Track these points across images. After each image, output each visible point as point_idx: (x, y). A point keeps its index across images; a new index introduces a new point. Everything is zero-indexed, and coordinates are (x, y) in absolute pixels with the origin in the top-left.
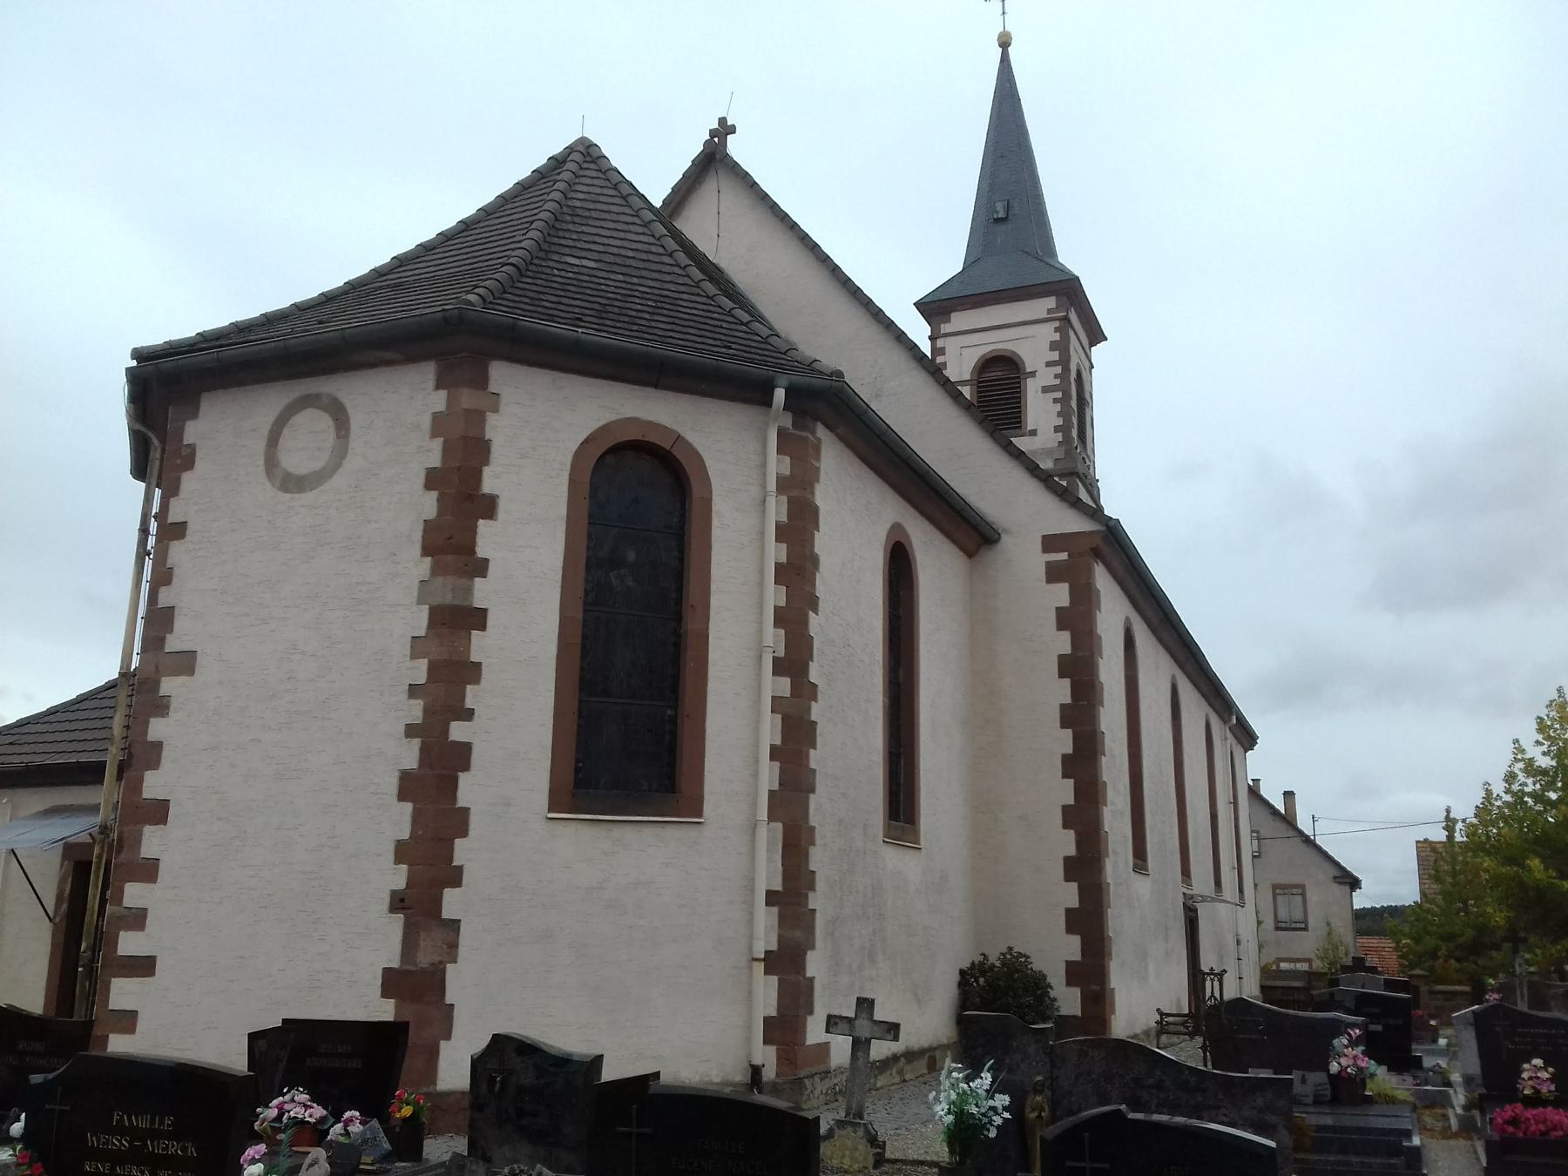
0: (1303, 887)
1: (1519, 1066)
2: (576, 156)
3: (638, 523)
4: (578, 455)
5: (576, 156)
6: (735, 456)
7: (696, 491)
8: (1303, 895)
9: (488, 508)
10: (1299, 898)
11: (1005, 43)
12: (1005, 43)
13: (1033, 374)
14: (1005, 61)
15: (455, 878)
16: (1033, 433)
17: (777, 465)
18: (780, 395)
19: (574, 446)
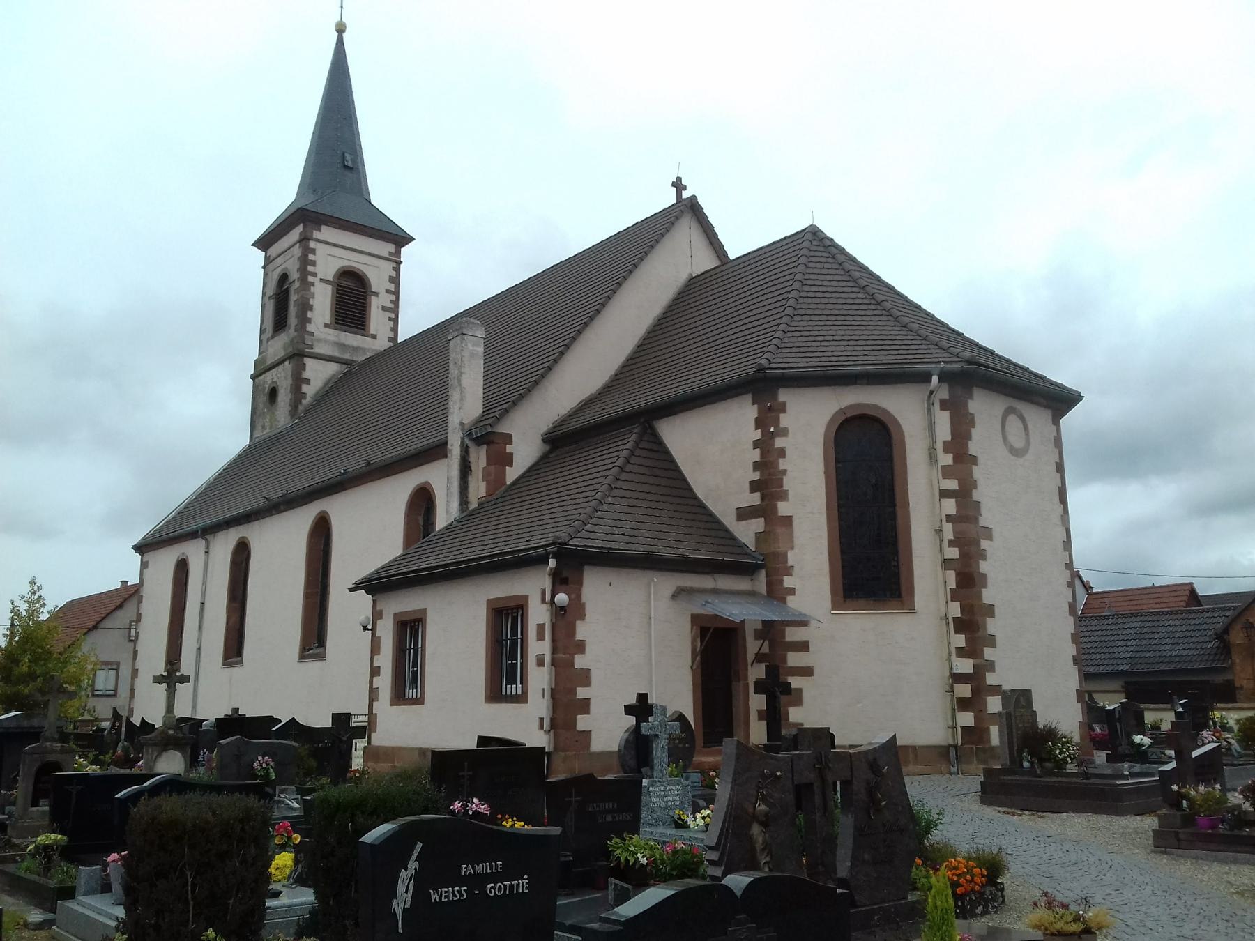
0: (118, 664)
1: (487, 802)
2: (808, 236)
3: (865, 456)
4: (832, 420)
5: (808, 236)
6: (913, 415)
7: (895, 437)
8: (117, 670)
9: (974, 460)
10: (113, 673)
11: (341, 29)
12: (341, 29)
13: (376, 294)
14: (340, 44)
15: (581, 647)
16: (374, 337)
17: (943, 420)
18: (935, 379)
19: (833, 412)
